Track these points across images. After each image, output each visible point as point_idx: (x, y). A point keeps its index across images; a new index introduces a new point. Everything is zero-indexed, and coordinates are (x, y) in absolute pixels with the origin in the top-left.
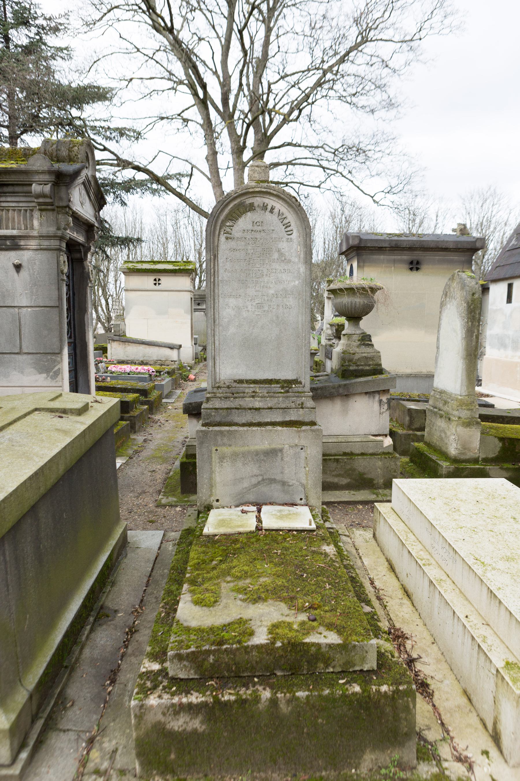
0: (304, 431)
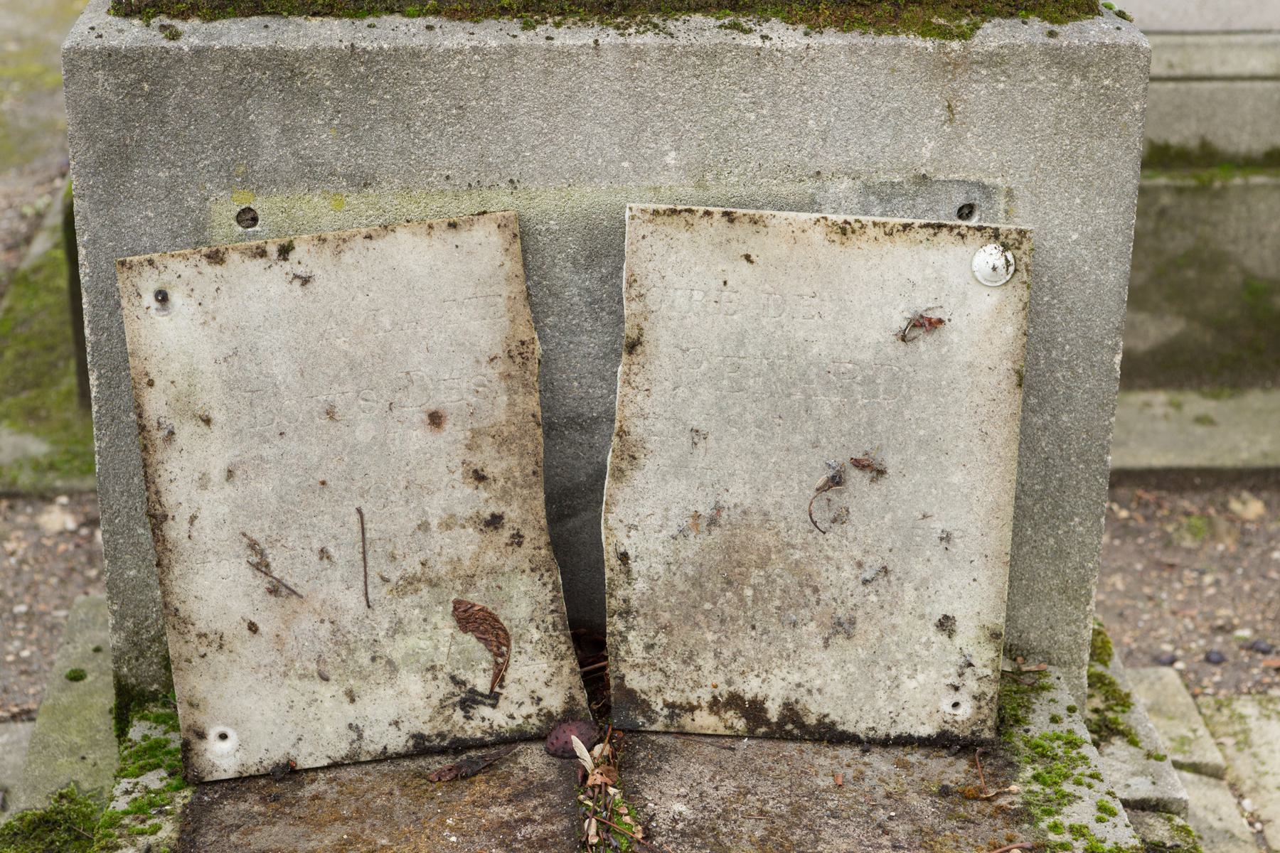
0: (994, 61)
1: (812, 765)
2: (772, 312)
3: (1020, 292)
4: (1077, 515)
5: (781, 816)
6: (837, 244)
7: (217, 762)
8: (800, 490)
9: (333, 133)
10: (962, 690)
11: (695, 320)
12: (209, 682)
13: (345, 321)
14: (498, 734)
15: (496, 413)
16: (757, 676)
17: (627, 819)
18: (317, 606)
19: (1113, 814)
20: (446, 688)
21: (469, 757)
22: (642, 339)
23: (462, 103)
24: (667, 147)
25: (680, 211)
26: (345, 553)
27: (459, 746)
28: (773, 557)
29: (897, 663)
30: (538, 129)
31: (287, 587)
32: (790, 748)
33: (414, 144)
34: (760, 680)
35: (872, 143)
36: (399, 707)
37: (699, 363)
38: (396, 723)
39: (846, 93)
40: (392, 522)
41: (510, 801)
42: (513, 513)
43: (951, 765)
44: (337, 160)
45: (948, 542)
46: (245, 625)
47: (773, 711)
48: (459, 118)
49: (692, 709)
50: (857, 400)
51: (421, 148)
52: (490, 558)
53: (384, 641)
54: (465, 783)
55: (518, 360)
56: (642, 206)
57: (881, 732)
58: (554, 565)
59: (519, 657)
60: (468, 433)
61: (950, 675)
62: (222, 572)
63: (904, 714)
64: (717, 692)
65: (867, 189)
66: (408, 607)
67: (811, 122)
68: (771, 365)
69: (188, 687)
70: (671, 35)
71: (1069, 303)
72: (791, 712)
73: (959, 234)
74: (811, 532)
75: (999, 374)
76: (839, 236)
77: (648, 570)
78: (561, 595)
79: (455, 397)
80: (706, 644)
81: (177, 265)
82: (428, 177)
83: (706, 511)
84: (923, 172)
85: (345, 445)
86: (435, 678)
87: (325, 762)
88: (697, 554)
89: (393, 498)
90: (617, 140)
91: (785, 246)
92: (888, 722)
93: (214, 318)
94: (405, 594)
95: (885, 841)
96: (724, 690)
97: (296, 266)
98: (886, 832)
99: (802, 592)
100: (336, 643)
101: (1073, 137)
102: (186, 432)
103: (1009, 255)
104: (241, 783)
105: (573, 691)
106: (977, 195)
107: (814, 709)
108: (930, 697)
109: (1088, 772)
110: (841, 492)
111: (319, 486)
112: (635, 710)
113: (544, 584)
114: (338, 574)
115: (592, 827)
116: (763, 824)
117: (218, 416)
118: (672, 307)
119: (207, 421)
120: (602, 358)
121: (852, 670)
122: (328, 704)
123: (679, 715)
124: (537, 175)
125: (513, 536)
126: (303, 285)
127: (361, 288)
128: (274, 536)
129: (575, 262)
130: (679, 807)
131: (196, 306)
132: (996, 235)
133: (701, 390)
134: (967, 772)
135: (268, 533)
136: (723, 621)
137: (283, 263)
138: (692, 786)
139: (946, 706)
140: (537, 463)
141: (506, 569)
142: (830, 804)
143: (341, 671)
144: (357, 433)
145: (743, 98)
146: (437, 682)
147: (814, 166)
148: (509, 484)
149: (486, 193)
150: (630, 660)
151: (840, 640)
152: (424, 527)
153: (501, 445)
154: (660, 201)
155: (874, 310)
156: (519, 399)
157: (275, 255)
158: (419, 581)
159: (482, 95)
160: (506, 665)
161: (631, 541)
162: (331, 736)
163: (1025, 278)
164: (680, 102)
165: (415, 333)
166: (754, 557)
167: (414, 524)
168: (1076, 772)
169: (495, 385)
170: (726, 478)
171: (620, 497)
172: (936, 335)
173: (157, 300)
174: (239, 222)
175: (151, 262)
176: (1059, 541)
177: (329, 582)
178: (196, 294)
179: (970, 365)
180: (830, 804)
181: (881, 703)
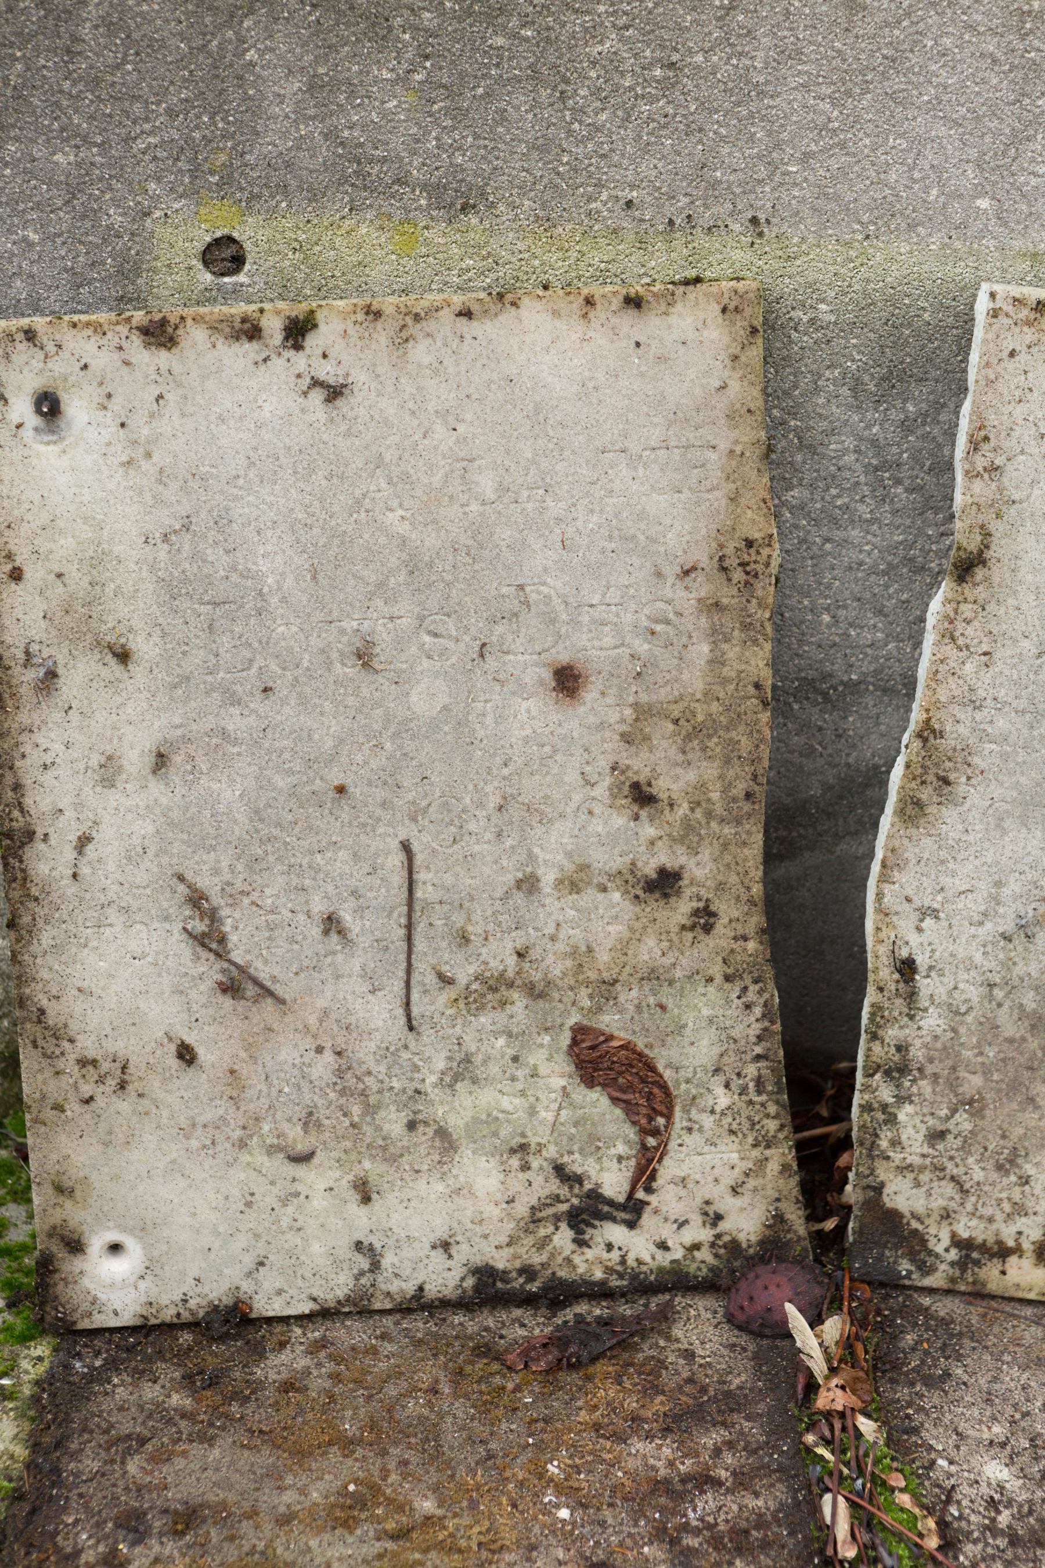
7: (102, 1297)
9: (411, 98)
12: (96, 1150)
13: (405, 478)
14: (635, 1276)
15: (686, 676)
17: (904, 1499)
18: (312, 1020)
20: (543, 1185)
21: (579, 1319)
22: (988, 554)
23: (675, 57)
26: (373, 925)
27: (558, 1294)
30: (821, 120)
31: (256, 982)
33: (570, 132)
36: (454, 1217)
38: (446, 1246)
40: (469, 871)
41: (667, 1430)
42: (700, 869)
44: (414, 153)
46: (173, 1048)
48: (666, 86)
49: (1003, 1252)
51: (582, 141)
52: (649, 950)
53: (435, 1094)
54: (574, 1378)
55: (738, 575)
56: (1016, 291)
58: (769, 973)
59: (687, 1139)
60: (628, 712)
62: (133, 946)
66: (485, 1034)
69: (54, 1157)
77: (950, 993)
78: (777, 1027)
79: (608, 641)
81: (82, 345)
82: (589, 200)
85: (388, 719)
86: (525, 1167)
87: (306, 1308)
89: (472, 826)
90: (973, 153)
93: (148, 455)
94: (481, 1008)
97: (317, 361)
100: (343, 1092)
102: (80, 673)
104: (145, 1339)
105: (783, 1205)
111: (332, 794)
113: (748, 1007)
114: (356, 965)
115: (836, 1512)
117: (144, 647)
119: (123, 656)
120: (885, 573)
122: (319, 1202)
123: (977, 1263)
124: (806, 211)
125: (696, 913)
126: (329, 400)
127: (443, 414)
128: (239, 885)
129: (857, 387)
131: (114, 428)
135: (227, 877)
137: (291, 353)
138: (1013, 1422)
140: (755, 777)
141: (678, 973)
143: (348, 1144)
144: (414, 698)
146: (528, 1175)
148: (698, 814)
149: (702, 240)
150: (897, 1157)
152: (528, 884)
153: (688, 738)
156: (732, 652)
157: (278, 338)
158: (511, 985)
159: (718, 42)
160: (662, 1150)
161: (924, 939)
162: (321, 1261)
165: (542, 510)
167: (510, 878)
169: (688, 623)
171: (910, 853)
173: (39, 411)
174: (206, 263)
175: (30, 335)
177: (338, 977)
178: (117, 404)
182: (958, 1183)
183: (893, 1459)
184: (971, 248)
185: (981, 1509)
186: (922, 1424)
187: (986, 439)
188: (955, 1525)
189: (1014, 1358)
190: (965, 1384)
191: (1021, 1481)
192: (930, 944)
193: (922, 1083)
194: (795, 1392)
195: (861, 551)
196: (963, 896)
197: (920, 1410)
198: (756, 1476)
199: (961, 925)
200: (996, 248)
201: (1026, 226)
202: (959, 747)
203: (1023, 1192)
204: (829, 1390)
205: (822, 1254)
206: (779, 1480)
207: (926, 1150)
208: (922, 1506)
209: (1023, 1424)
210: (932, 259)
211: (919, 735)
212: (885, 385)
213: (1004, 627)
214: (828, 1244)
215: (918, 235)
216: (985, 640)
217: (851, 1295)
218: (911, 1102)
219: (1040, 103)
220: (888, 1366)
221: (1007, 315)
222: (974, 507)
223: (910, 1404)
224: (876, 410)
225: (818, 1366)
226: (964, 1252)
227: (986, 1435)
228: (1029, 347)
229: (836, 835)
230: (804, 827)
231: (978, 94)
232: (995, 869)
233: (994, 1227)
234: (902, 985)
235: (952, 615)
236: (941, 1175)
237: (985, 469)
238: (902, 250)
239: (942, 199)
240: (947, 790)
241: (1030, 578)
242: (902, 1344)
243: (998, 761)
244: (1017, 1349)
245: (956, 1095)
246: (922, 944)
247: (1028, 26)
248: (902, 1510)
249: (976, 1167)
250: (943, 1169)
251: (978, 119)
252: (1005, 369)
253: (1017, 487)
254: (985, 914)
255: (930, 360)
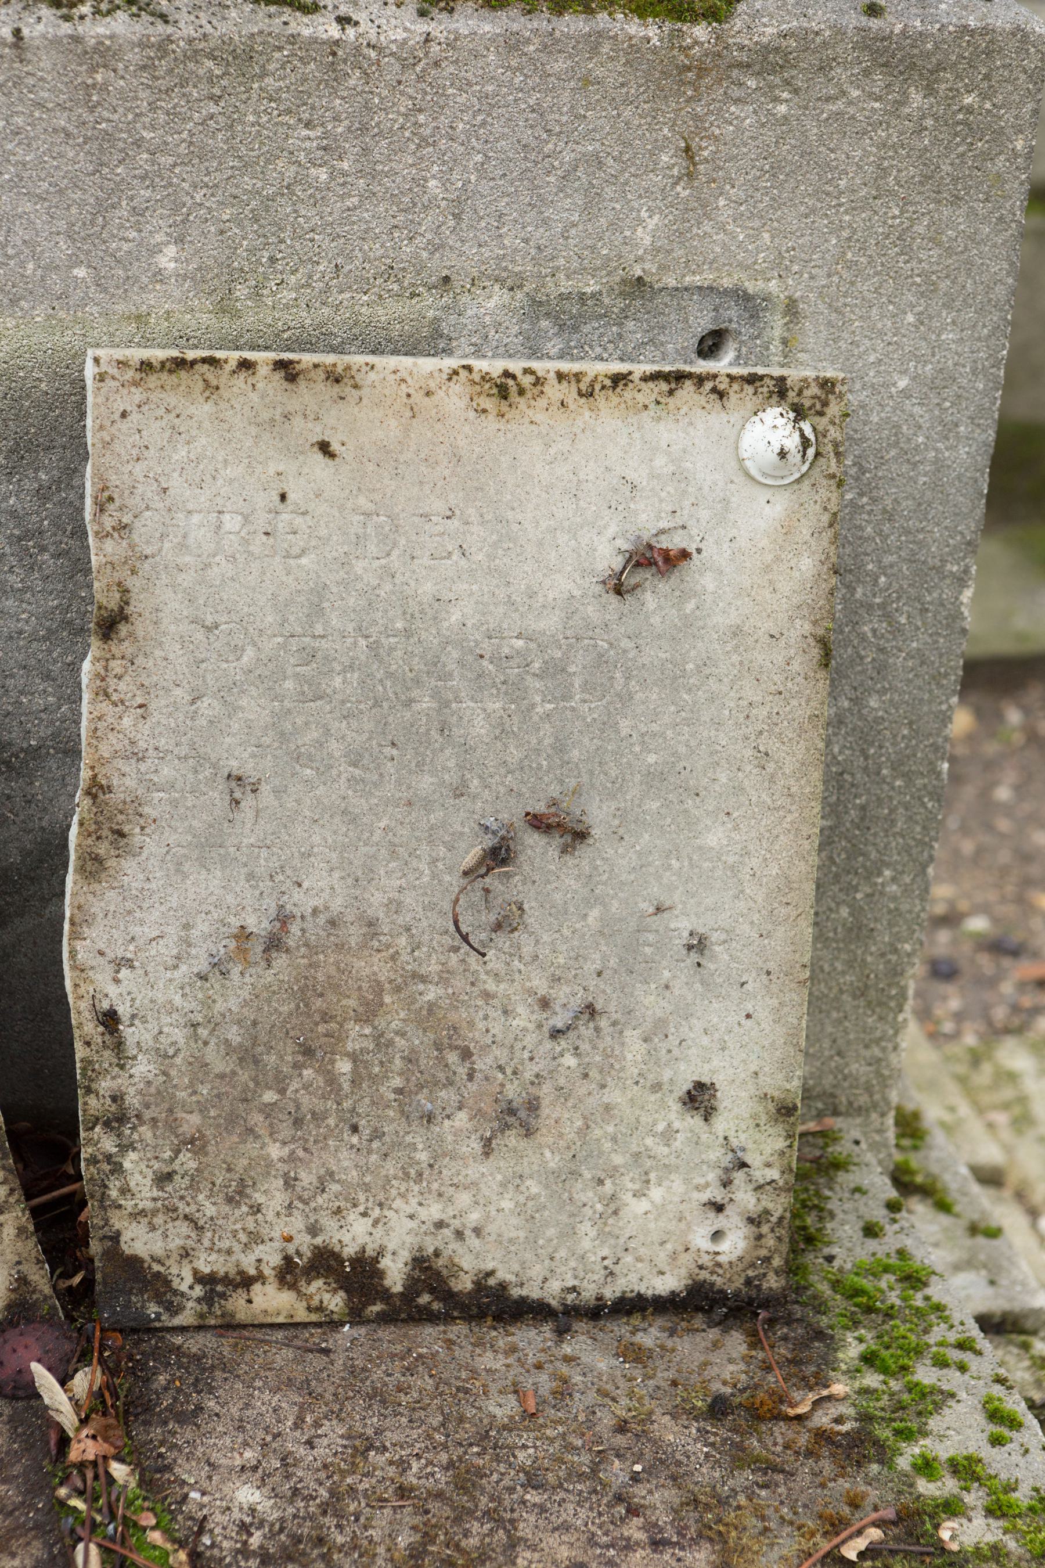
1: (474, 1373)
2: (373, 549)
3: (824, 494)
4: (888, 865)
5: (439, 1495)
6: (491, 417)
8: (434, 876)
10: (729, 1210)
11: (228, 569)
16: (364, 1214)
19: (1014, 1424)
22: (129, 610)
24: (159, 238)
25: (193, 363)
28: (387, 999)
29: (614, 1172)
32: (429, 1338)
34: (369, 1221)
35: (545, 222)
37: (238, 651)
39: (498, 128)
43: (716, 1345)
45: (701, 952)
47: (395, 1273)
49: (246, 1282)
50: (533, 706)
56: (119, 354)
57: (589, 1293)
61: (707, 1185)
63: (628, 1259)
64: (291, 1249)
65: (537, 307)
67: (432, 183)
68: (374, 648)
70: (164, 18)
71: (888, 502)
72: (426, 1272)
73: (714, 390)
74: (456, 949)
75: (788, 646)
76: (495, 400)
77: (156, 1039)
80: (269, 1164)
83: (258, 924)
84: (639, 273)
88: (246, 1003)
90: (62, 225)
91: (393, 423)
92: (599, 1275)
95: (634, 1529)
96: (304, 1243)
98: (633, 1511)
99: (440, 1059)
101: (906, 202)
103: (806, 427)
105: (23, 1268)
106: (733, 313)
107: (469, 1263)
108: (672, 1226)
109: (952, 1337)
110: (508, 876)
112: (141, 1292)
116: (408, 1517)
118: (182, 547)
120: (45, 639)
121: (535, 1190)
123: (223, 1296)
130: (248, 1495)
132: (781, 390)
133: (244, 702)
134: (747, 1359)
136: (298, 1122)
138: (264, 1445)
139: (700, 1240)
142: (521, 1455)
145: (304, 139)
147: (437, 265)
150: (128, 1204)
151: (512, 1139)
154: (147, 342)
155: (562, 538)
161: (123, 989)
163: (833, 467)
164: (183, 149)
166: (352, 1003)
168: (932, 1339)
170: (296, 862)
171: (97, 908)
172: (674, 578)
176: (856, 911)
179: (737, 632)
180: (521, 1455)
181: (586, 1244)
182: (192, 1221)
183: (145, 1499)
184: (75, 316)
185: (233, 1534)
186: (175, 1460)
187: (111, 499)
188: (208, 1554)
189: (265, 1383)
190: (217, 1415)
191: (272, 1501)
192: (129, 993)
193: (142, 1129)
194: (49, 1450)
195: (18, 620)
196: (154, 943)
197: (174, 1447)
198: (12, 1538)
199: (157, 971)
200: (100, 314)
201: (126, 290)
202: (128, 799)
203: (256, 1221)
204: (79, 1441)
205: (73, 1309)
206: (35, 1537)
207: (156, 1193)
208: (174, 1541)
209: (274, 1445)
210: (39, 330)
211: (88, 793)
212: (15, 457)
213: (155, 678)
214: (79, 1299)
215: (22, 309)
216: (138, 693)
217: (101, 1345)
218: (134, 1149)
219: (119, 171)
220: (139, 1410)
221: (113, 378)
222: (109, 566)
223: (162, 1443)
224: (9, 482)
225: (67, 1417)
226: (208, 1287)
227: (238, 1462)
228: (139, 407)
229: (42, 899)
230: (10, 894)
231: (57, 168)
232: (181, 913)
233: (234, 1258)
234: (107, 1037)
235: (103, 673)
236: (174, 1215)
237: (114, 528)
238: (9, 325)
239: (39, 272)
240: (122, 842)
241: (173, 628)
242: (155, 1386)
243: (168, 808)
244: (268, 1373)
245: (177, 1136)
246: (121, 995)
247: (95, 98)
248: (155, 1547)
249: (207, 1203)
250: (176, 1210)
251: (61, 192)
252: (119, 430)
253: (148, 542)
254: (178, 958)
255: (54, 428)
